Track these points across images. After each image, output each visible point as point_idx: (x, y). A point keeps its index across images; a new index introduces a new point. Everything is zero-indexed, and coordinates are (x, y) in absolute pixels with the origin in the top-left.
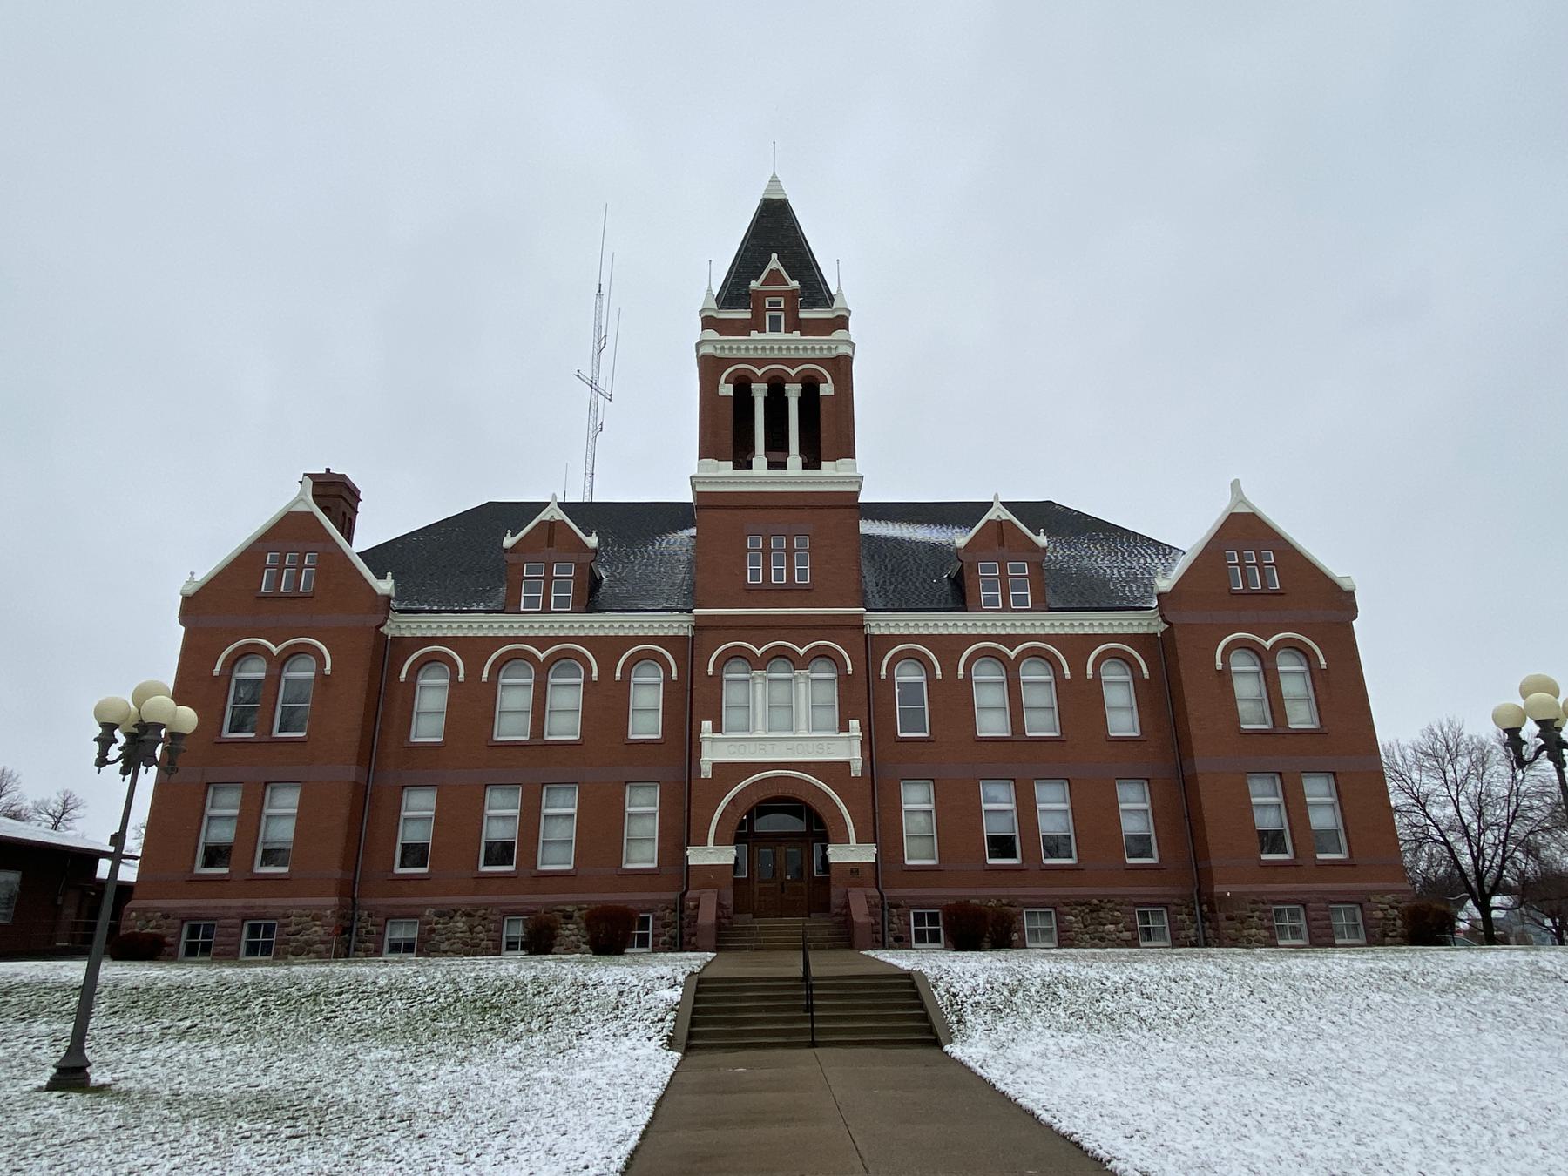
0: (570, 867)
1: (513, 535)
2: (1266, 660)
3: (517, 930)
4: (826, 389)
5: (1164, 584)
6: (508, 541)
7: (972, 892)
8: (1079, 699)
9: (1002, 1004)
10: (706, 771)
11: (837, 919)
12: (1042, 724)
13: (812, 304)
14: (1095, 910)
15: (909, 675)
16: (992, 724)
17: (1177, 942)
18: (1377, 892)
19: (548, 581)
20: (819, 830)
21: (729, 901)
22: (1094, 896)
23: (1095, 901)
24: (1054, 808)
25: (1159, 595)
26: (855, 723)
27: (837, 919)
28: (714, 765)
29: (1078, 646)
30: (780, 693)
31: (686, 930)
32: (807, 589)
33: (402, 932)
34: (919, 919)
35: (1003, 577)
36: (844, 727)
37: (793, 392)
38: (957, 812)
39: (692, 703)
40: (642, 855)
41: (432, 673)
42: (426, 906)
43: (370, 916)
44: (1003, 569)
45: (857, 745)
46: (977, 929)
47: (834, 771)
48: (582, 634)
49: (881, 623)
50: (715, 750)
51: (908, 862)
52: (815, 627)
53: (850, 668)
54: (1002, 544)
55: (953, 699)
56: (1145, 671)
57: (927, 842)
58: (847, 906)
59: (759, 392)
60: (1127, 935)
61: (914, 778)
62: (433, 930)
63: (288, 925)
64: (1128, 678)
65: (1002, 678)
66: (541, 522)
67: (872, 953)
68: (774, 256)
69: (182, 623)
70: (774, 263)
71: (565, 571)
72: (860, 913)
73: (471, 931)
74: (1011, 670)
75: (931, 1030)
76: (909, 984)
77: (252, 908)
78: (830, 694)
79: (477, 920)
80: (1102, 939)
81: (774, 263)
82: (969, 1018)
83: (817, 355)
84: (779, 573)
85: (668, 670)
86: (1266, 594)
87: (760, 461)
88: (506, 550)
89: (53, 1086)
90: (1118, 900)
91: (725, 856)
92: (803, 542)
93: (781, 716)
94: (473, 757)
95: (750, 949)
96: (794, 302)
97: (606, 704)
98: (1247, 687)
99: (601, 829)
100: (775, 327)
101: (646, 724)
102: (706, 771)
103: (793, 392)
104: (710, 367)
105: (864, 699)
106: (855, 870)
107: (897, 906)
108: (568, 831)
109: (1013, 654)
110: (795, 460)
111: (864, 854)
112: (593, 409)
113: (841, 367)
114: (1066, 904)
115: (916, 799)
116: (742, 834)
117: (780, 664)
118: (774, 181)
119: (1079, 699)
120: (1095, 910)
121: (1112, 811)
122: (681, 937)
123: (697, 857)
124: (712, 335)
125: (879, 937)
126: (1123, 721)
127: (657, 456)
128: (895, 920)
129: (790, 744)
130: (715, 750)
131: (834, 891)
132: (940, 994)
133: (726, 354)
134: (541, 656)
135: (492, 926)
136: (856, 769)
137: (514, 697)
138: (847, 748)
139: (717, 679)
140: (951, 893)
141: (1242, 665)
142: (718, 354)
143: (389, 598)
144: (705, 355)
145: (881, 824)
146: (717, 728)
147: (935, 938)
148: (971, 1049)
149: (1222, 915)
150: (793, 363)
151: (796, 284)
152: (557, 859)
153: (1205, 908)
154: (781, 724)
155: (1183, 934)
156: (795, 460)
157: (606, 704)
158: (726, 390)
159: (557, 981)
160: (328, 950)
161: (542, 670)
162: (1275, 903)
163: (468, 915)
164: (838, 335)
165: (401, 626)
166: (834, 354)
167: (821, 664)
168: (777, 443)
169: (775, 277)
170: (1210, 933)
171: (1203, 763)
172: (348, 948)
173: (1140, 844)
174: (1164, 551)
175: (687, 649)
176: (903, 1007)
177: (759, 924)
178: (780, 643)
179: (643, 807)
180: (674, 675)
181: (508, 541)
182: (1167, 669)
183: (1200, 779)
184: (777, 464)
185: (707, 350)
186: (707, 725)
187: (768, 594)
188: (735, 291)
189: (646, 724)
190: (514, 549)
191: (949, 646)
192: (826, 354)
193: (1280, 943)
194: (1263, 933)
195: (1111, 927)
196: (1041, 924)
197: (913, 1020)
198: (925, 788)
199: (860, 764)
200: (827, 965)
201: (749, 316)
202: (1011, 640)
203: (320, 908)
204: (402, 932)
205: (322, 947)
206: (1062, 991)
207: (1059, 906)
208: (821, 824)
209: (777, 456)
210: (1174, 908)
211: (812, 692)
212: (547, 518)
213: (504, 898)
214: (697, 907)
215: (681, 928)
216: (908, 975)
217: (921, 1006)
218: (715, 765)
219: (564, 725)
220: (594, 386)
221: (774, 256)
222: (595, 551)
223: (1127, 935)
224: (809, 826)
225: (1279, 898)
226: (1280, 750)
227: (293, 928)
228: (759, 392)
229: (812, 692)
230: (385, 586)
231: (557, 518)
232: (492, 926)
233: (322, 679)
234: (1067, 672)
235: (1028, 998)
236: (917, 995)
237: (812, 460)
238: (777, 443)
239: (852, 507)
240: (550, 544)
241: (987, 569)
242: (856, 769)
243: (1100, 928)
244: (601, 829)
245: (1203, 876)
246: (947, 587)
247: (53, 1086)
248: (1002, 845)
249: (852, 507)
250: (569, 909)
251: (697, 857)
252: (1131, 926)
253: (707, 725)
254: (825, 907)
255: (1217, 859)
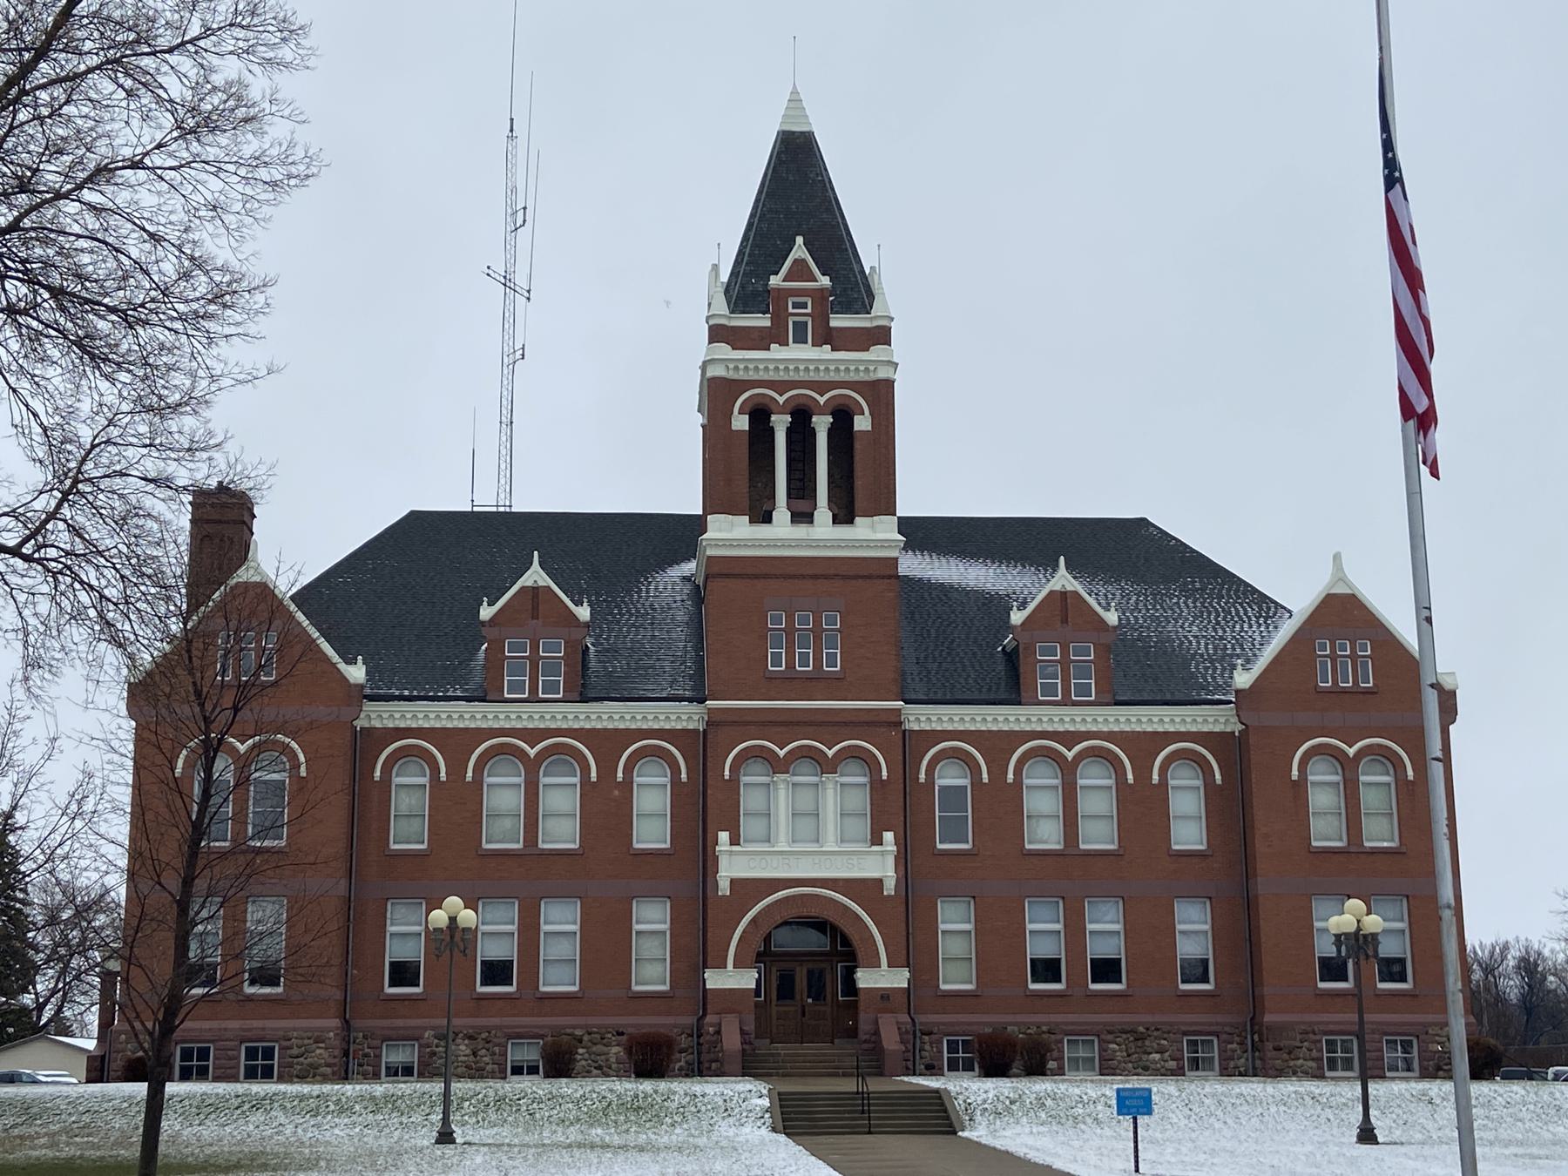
0: (575, 988)
1: (490, 604)
2: (1348, 767)
3: (529, 1053)
4: (862, 423)
5: (1243, 679)
6: (486, 612)
7: (1009, 1018)
8: (1142, 807)
9: (997, 1113)
10: (724, 888)
11: (865, 1046)
12: (1099, 836)
13: (847, 307)
14: (1140, 1038)
15: (951, 777)
16: (1045, 835)
17: (1227, 1072)
18: (1435, 1024)
19: (534, 661)
20: (845, 952)
21: (750, 1027)
22: (1140, 1024)
23: (1141, 1029)
24: (1106, 929)
25: (1238, 692)
26: (889, 836)
27: (865, 1046)
28: (732, 881)
29: (1143, 745)
30: (805, 800)
31: (705, 1057)
32: (836, 678)
33: (396, 1056)
34: (953, 1047)
35: (1065, 662)
36: (877, 840)
37: (822, 424)
38: (998, 935)
39: (705, 810)
40: (652, 973)
41: (412, 768)
42: (426, 1029)
43: (365, 1037)
44: (1065, 652)
45: (891, 861)
46: (996, 1059)
47: (865, 889)
48: (576, 726)
49: (921, 718)
50: (734, 864)
51: (943, 987)
52: (846, 724)
53: (885, 773)
54: (1065, 621)
55: (1000, 805)
56: (1218, 776)
57: (965, 964)
58: (877, 1033)
59: (781, 424)
60: (1172, 1064)
61: (952, 895)
62: (434, 1054)
63: (290, 1048)
64: (1199, 783)
65: (1057, 782)
66: (523, 588)
67: (906, 1079)
68: (800, 240)
69: (131, 716)
70: (799, 250)
71: (554, 651)
72: (891, 1040)
73: (475, 1054)
74: (1068, 772)
75: (951, 1125)
76: (937, 1099)
77: (250, 1030)
78: (860, 800)
79: (481, 1044)
80: (1146, 1069)
81: (799, 250)
82: (978, 1118)
83: (853, 377)
84: (804, 657)
85: (675, 770)
86: (1355, 692)
87: (782, 513)
88: (483, 623)
89: (437, 1142)
90: (1166, 1028)
91: (746, 980)
92: (833, 623)
93: (806, 825)
94: (459, 860)
95: (777, 1075)
96: (825, 304)
97: (607, 809)
98: (1323, 798)
99: (606, 945)
100: (800, 339)
101: (652, 828)
102: (724, 888)
103: (822, 424)
104: (718, 394)
105: (899, 807)
106: (885, 995)
107: (929, 1034)
108: (570, 949)
109: (1070, 755)
110: (823, 513)
111: (899, 979)
112: (508, 320)
113: (881, 394)
114: (1110, 1032)
115: (954, 922)
116: (763, 955)
117: (806, 765)
118: (795, 100)
119: (1142, 807)
120: (1140, 1038)
121: (1168, 931)
122: (700, 1063)
123: (715, 980)
124: (724, 351)
125: (910, 1064)
126: (1188, 830)
127: (616, 438)
128: (927, 1047)
129: (817, 859)
130: (734, 864)
131: (862, 1016)
132: (959, 1104)
133: (742, 375)
134: (532, 752)
135: (497, 1049)
136: (890, 888)
137: (503, 794)
138: (879, 864)
139: (734, 783)
140: (985, 1021)
141: (1322, 775)
142: (732, 375)
143: (362, 686)
144: (713, 380)
145: (915, 948)
146: (735, 841)
147: (968, 1068)
148: (978, 1132)
149: (1269, 1045)
150: (822, 387)
151: (825, 281)
152: (559, 979)
153: (1256, 1037)
154: (805, 837)
155: (1232, 1064)
156: (823, 513)
157: (607, 809)
158: (741, 423)
159: (675, 1093)
160: (334, 1073)
161: (532, 768)
162: (1326, 1033)
163: (471, 1038)
164: (877, 352)
165: (378, 716)
166: (872, 377)
167: (853, 766)
168: (801, 488)
169: (800, 271)
170: (1258, 1063)
171: (1265, 886)
172: (346, 1072)
173: (1198, 970)
174: (1267, 609)
175: (700, 748)
176: (937, 1125)
177: (781, 1049)
178: (807, 742)
179: (652, 919)
180: (684, 776)
181: (486, 612)
182: (1243, 778)
183: (1261, 900)
184: (802, 516)
185: (716, 371)
186: (724, 836)
187: (792, 684)
188: (748, 285)
189: (652, 828)
190: (493, 621)
191: (997, 745)
192: (862, 377)
193: (1328, 1074)
194: (1310, 1063)
195: (1157, 1056)
196: (1082, 1053)
197: (938, 1118)
198: (963, 907)
199: (893, 883)
200: (875, 1085)
201: (768, 324)
202: (1069, 739)
203: (322, 1030)
204: (396, 1056)
205: (329, 1070)
206: (1049, 1102)
207: (1104, 1034)
208: (846, 941)
209: (802, 505)
210: (1224, 1037)
211: (840, 798)
212: (530, 583)
213: (508, 1021)
214: (718, 1032)
215: (699, 1053)
216: (937, 1091)
217: (945, 1111)
218: (734, 882)
219: (562, 831)
220: (507, 283)
221: (800, 240)
222: (587, 625)
223: (1172, 1064)
224: (834, 941)
225: (1331, 1027)
226: (1354, 869)
227: (295, 1051)
228: (781, 424)
229: (840, 798)
230: (356, 673)
231: (541, 583)
232: (497, 1049)
233: (300, 784)
234: (1130, 776)
235: (1023, 1104)
236: (943, 1104)
237: (844, 515)
238: (801, 488)
239: (890, 577)
240: (535, 616)
241: (1046, 655)
242: (890, 888)
243: (1145, 1057)
244: (606, 945)
245: (1257, 1004)
246: (1001, 667)
247: (437, 1142)
248: (1047, 969)
249: (890, 577)
250: (578, 1032)
251: (715, 980)
252: (1178, 1055)
253: (724, 836)
254: (852, 1033)
255: (1268, 990)
